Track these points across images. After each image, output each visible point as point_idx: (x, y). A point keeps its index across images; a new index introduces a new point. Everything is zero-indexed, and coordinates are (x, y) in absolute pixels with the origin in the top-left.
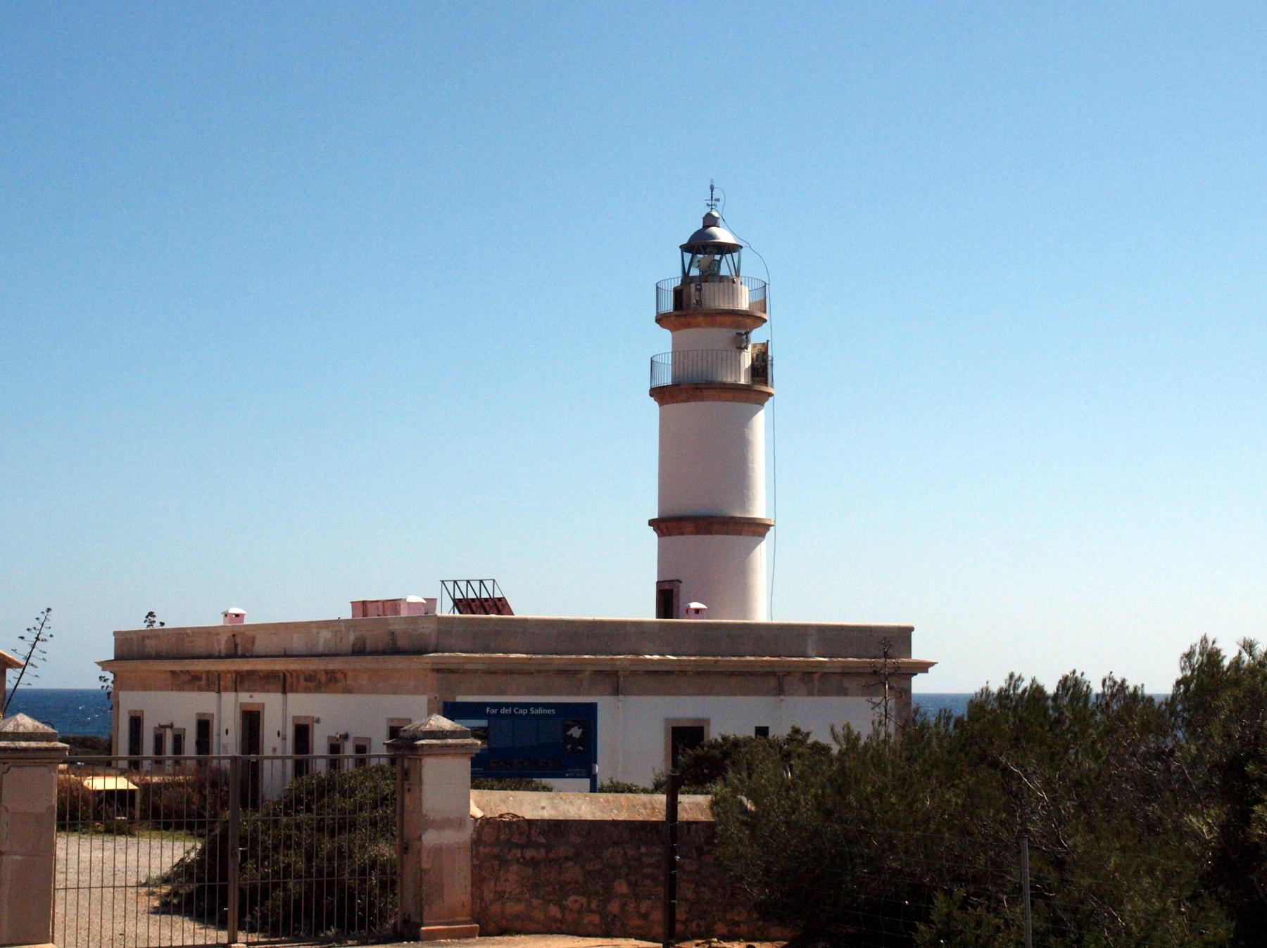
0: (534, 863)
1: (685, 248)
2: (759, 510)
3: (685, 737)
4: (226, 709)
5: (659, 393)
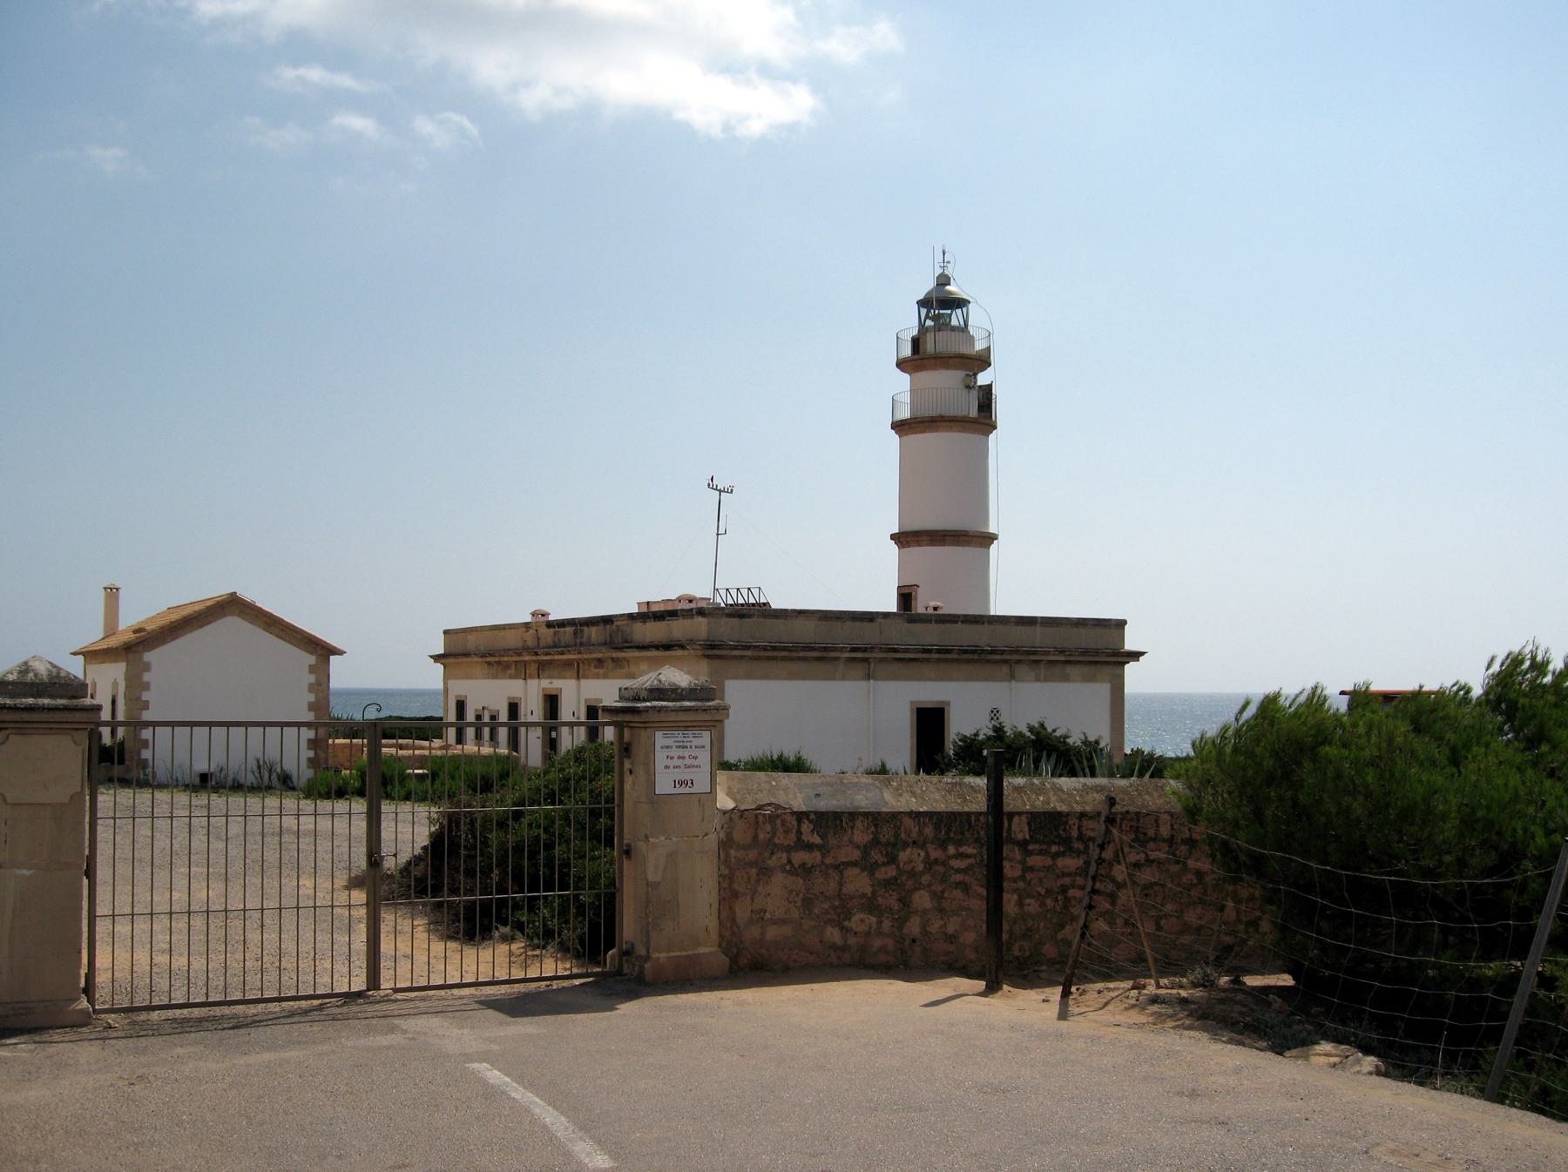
0: (806, 871)
1: (921, 303)
3: (930, 722)
4: (530, 694)
5: (900, 427)
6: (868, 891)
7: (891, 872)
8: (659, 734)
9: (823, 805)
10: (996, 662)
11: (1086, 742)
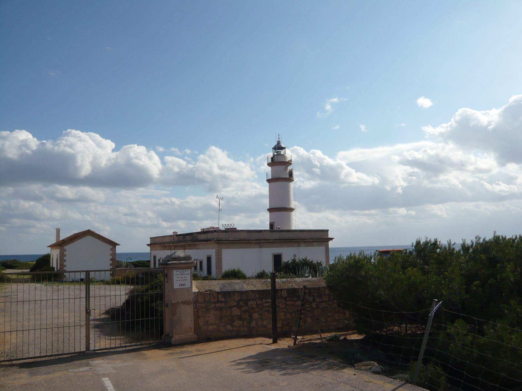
0: (220, 309)
2: (292, 206)
3: (277, 258)
5: (269, 181)
6: (239, 314)
7: (246, 308)
8: (175, 271)
9: (225, 290)
10: (295, 242)
11: (317, 263)
